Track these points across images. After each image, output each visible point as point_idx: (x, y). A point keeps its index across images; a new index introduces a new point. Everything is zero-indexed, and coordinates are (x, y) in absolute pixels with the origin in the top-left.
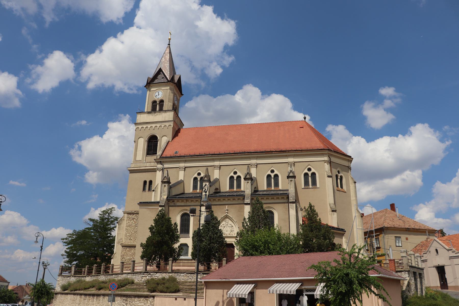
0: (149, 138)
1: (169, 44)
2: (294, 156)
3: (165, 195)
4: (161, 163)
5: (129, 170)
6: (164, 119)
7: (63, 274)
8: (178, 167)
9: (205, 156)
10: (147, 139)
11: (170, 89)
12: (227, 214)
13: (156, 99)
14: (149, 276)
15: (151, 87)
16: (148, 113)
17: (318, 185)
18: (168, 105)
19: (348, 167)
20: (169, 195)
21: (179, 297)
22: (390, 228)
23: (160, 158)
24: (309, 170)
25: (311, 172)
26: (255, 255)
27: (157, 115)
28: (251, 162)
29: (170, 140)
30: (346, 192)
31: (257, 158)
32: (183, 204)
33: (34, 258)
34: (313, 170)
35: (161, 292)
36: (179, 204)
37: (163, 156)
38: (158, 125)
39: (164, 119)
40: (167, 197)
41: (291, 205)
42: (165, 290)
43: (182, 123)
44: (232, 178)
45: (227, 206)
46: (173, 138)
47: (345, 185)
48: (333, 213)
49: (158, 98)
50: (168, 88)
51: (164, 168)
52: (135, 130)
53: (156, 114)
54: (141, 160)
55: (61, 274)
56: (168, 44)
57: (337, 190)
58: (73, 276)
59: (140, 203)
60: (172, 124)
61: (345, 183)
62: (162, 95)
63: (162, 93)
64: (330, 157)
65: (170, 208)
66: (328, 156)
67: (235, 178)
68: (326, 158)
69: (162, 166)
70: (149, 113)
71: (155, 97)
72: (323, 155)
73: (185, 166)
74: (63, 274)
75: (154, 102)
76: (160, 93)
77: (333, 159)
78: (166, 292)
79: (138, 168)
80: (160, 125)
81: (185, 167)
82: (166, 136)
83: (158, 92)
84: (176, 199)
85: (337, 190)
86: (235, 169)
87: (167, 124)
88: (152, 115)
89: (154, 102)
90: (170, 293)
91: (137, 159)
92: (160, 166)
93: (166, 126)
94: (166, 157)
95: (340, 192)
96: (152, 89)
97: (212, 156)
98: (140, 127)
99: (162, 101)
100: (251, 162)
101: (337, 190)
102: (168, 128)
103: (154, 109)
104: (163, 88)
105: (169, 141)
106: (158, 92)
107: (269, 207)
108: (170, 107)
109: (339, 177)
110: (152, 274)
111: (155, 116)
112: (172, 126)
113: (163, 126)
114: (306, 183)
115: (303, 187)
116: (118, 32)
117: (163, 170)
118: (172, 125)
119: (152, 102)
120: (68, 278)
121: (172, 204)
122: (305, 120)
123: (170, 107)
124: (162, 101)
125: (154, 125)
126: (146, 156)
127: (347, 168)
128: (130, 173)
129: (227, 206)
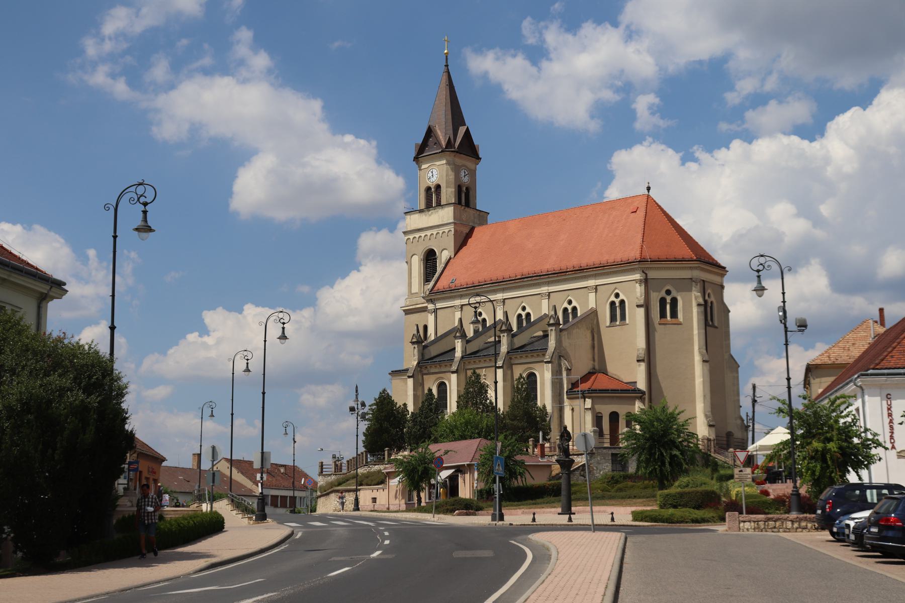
0: (426, 255)
1: (447, 66)
2: (595, 276)
3: (415, 361)
4: (431, 301)
5: (404, 310)
6: (442, 221)
7: (324, 473)
8: (540, 294)
9: (484, 286)
10: (422, 257)
11: (448, 163)
12: (484, 380)
13: (430, 184)
14: (369, 469)
15: (421, 162)
16: (419, 212)
17: (627, 321)
18: (448, 194)
19: (691, 279)
20: (423, 358)
21: (380, 488)
22: (822, 366)
23: (429, 294)
24: (617, 295)
25: (619, 299)
26: (446, 442)
27: (432, 213)
28: (542, 291)
29: (452, 256)
30: (682, 322)
31: (549, 283)
32: (436, 370)
33: (319, 449)
34: (622, 297)
35: (368, 485)
36: (433, 370)
37: (436, 288)
38: (434, 232)
39: (442, 221)
40: (418, 363)
41: (546, 366)
42: (369, 483)
43: (481, 214)
44: (613, 303)
45: (484, 370)
46: (456, 253)
47: (682, 311)
48: (638, 364)
49: (432, 181)
50: (444, 162)
51: (437, 309)
52: (406, 243)
53: (430, 212)
54: (417, 291)
55: (322, 472)
56: (445, 66)
57: (659, 324)
58: (334, 475)
59: (392, 371)
60: (452, 227)
61: (681, 309)
62: (437, 176)
63: (437, 173)
64: (646, 272)
65: (424, 376)
66: (641, 272)
67: (617, 304)
68: (637, 276)
69: (433, 305)
70: (421, 211)
71: (428, 182)
72: (632, 271)
73: (462, 304)
74: (324, 473)
75: (428, 189)
76: (435, 172)
77: (652, 274)
78: (370, 485)
79: (414, 307)
80: (443, 231)
81: (462, 305)
82: (444, 249)
83: (431, 170)
84: (428, 365)
85: (659, 324)
86: (616, 289)
87: (446, 229)
88: (426, 215)
89: (428, 189)
90: (374, 485)
91: (413, 292)
92: (431, 306)
93: (444, 232)
94: (438, 292)
95: (668, 326)
96: (424, 166)
97: (492, 285)
98: (411, 237)
99: (438, 187)
100: (542, 291)
101: (658, 325)
102: (430, 239)
103: (429, 206)
104: (438, 163)
105: (450, 258)
106: (431, 170)
107: (530, 368)
108: (450, 196)
109: (668, 301)
110: (371, 466)
111: (430, 215)
112: (453, 231)
113: (441, 232)
114: (613, 318)
115: (608, 324)
116: (196, 331)
117: (435, 311)
118: (453, 230)
119: (425, 190)
120: (329, 478)
121: (425, 371)
122: (649, 192)
123: (451, 195)
124: (438, 187)
125: (429, 233)
126: (424, 285)
127: (690, 280)
128: (406, 314)
129: (484, 370)
